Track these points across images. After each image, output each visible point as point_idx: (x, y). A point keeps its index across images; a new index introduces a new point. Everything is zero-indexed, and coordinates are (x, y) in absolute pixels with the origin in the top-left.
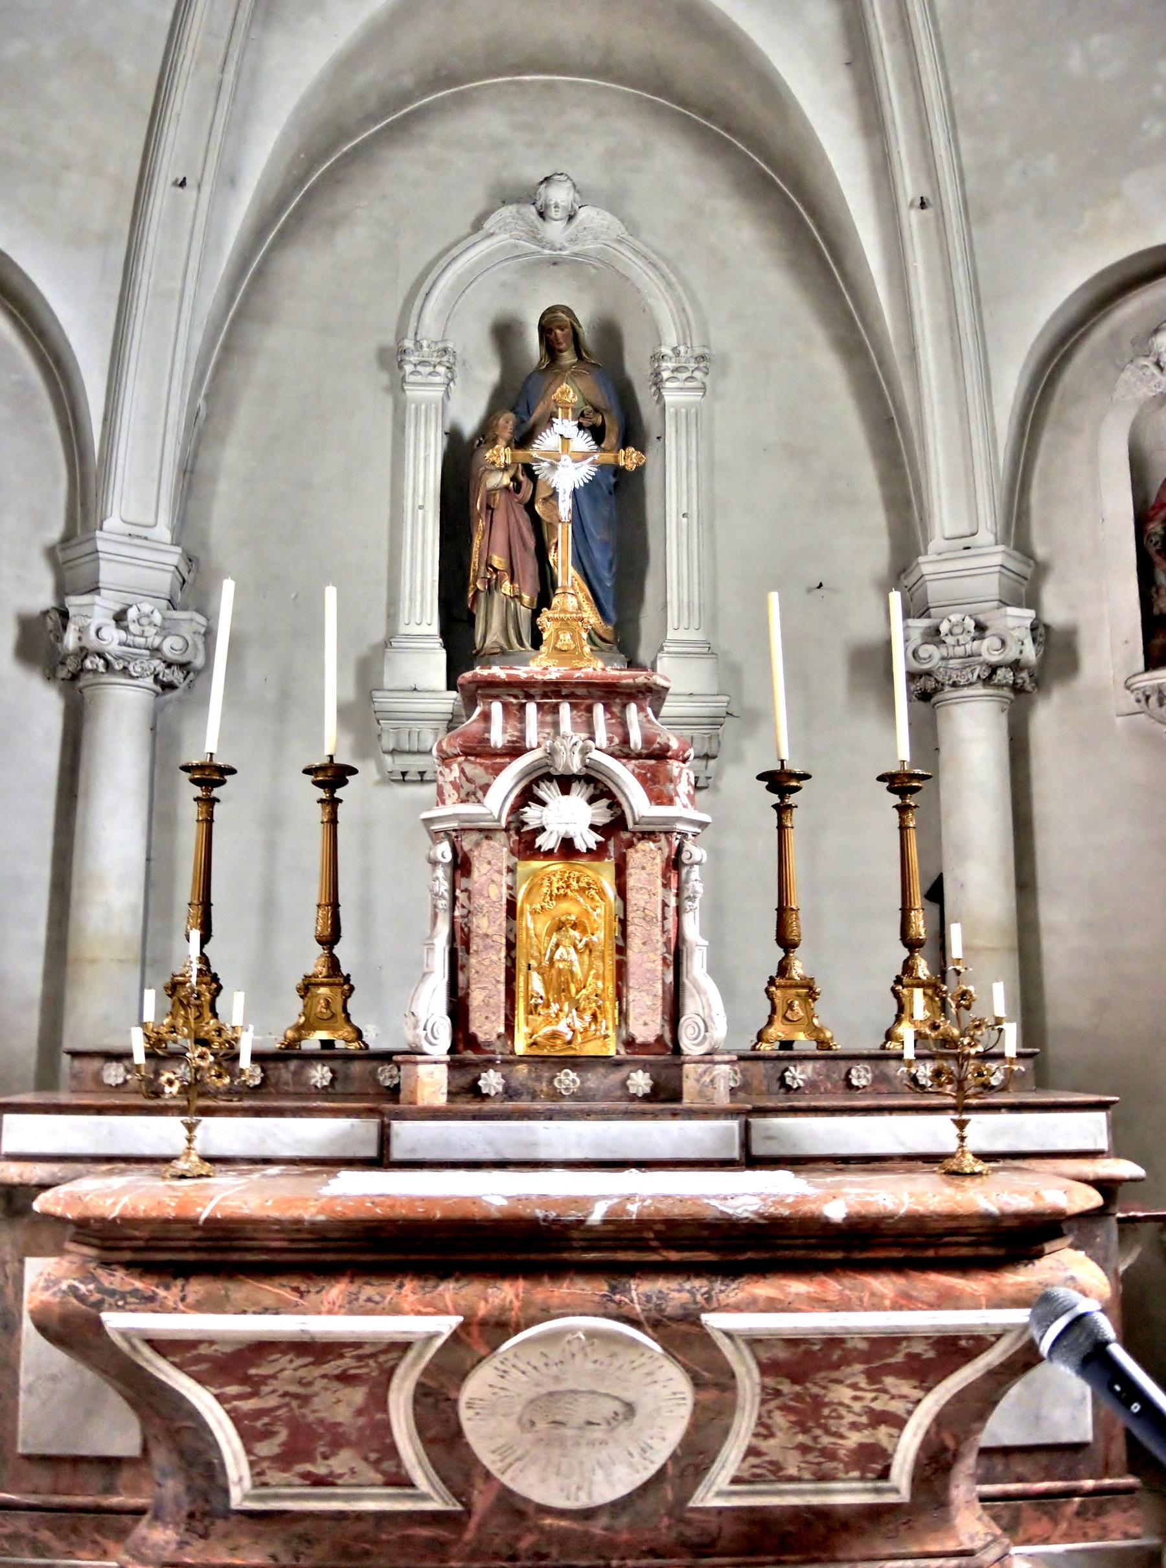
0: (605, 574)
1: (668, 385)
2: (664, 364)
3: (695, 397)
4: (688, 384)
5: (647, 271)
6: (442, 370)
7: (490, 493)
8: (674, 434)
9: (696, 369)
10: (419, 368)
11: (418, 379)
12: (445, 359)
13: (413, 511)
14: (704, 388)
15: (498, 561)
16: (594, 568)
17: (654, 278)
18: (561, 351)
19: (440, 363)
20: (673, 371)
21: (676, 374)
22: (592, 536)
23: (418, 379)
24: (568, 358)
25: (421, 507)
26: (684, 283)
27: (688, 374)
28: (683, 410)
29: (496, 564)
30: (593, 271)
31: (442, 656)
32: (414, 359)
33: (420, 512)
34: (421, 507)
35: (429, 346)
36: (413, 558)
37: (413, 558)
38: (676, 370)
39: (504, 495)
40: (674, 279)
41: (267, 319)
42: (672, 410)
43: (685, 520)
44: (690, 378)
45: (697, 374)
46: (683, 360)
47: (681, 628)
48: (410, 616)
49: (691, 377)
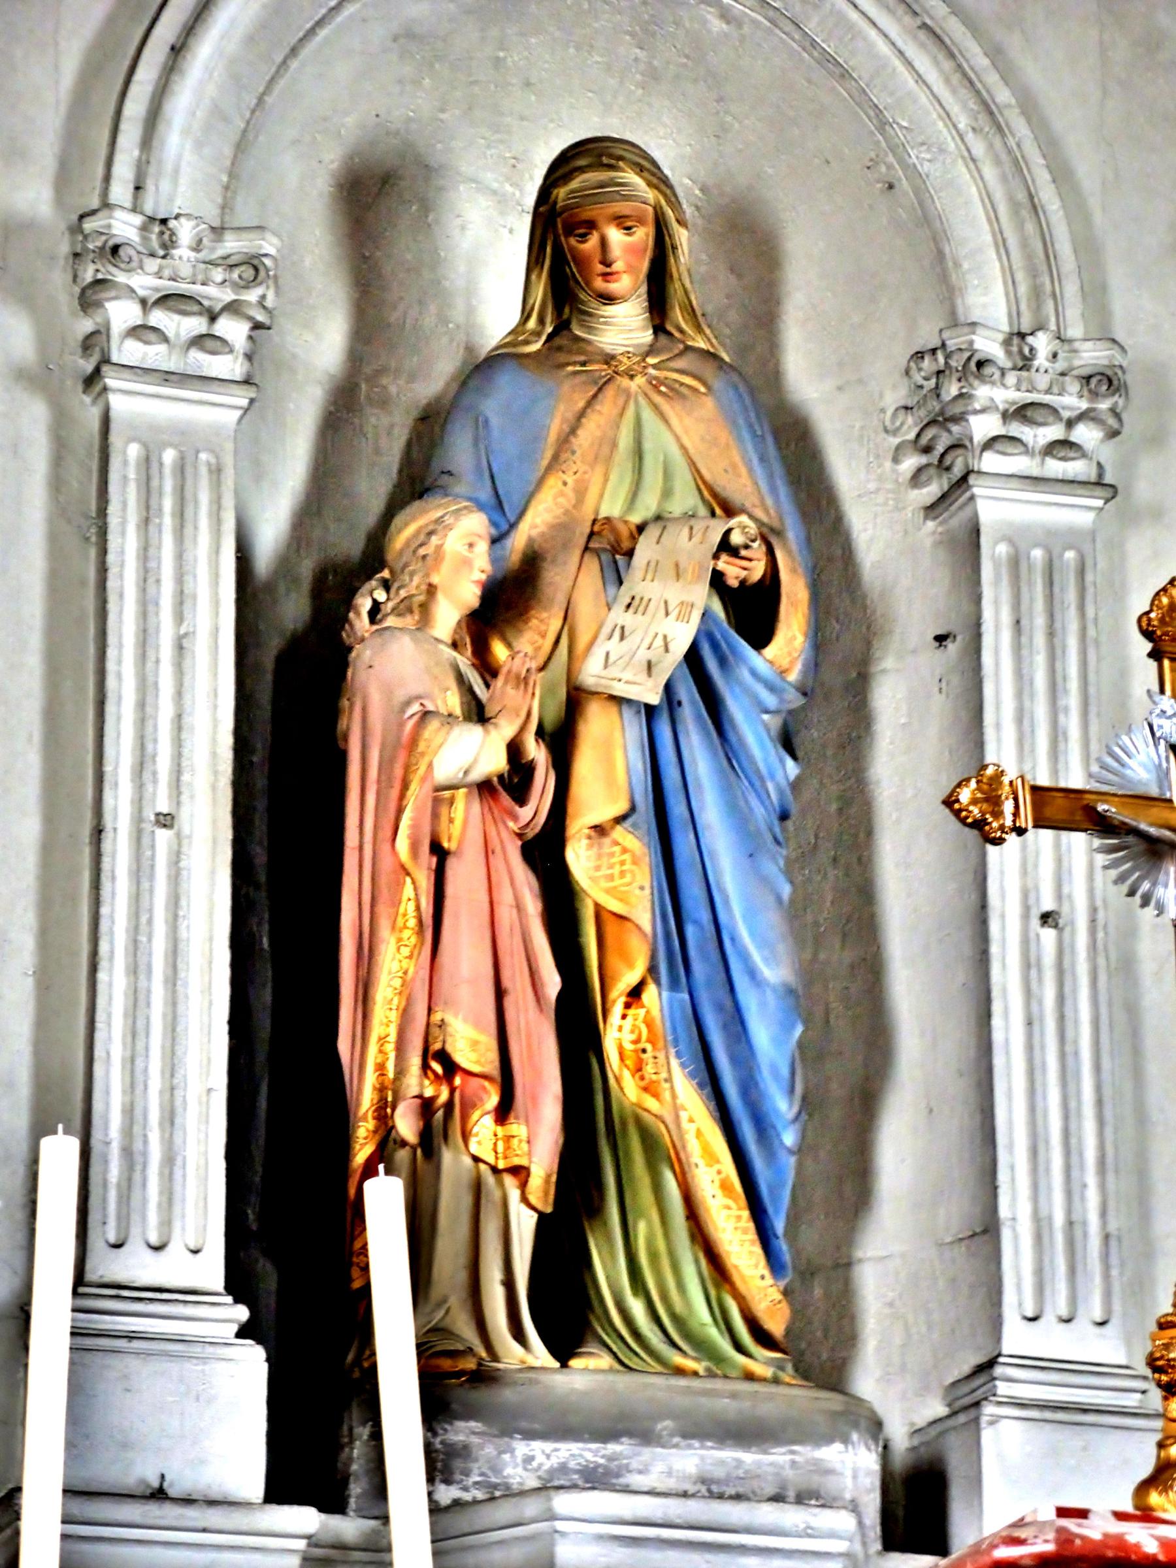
0: (782, 1106)
1: (990, 462)
2: (983, 393)
3: (1077, 513)
4: (1055, 467)
5: (911, 51)
6: (234, 330)
7: (441, 795)
8: (1006, 636)
9: (1083, 416)
10: (158, 318)
11: (153, 355)
12: (252, 296)
13: (138, 835)
14: (1099, 484)
15: (470, 1045)
16: (749, 1086)
17: (932, 76)
18: (608, 299)
19: (233, 308)
20: (1006, 416)
21: (1017, 429)
22: (752, 973)
23: (153, 355)
24: (622, 326)
25: (166, 821)
26: (1029, 106)
27: (1055, 432)
28: (1037, 554)
29: (463, 1057)
30: (717, 25)
31: (251, 1365)
32: (144, 282)
33: (163, 835)
34: (166, 821)
35: (197, 247)
36: (136, 1000)
37: (136, 1000)
38: (1022, 413)
39: (476, 807)
40: (1003, 96)
41: (962, 291)
42: (1002, 549)
43: (1048, 935)
44: (1062, 447)
45: (1086, 434)
46: (1042, 381)
47: (1049, 1319)
48: (166, 1224)
49: (1066, 443)
